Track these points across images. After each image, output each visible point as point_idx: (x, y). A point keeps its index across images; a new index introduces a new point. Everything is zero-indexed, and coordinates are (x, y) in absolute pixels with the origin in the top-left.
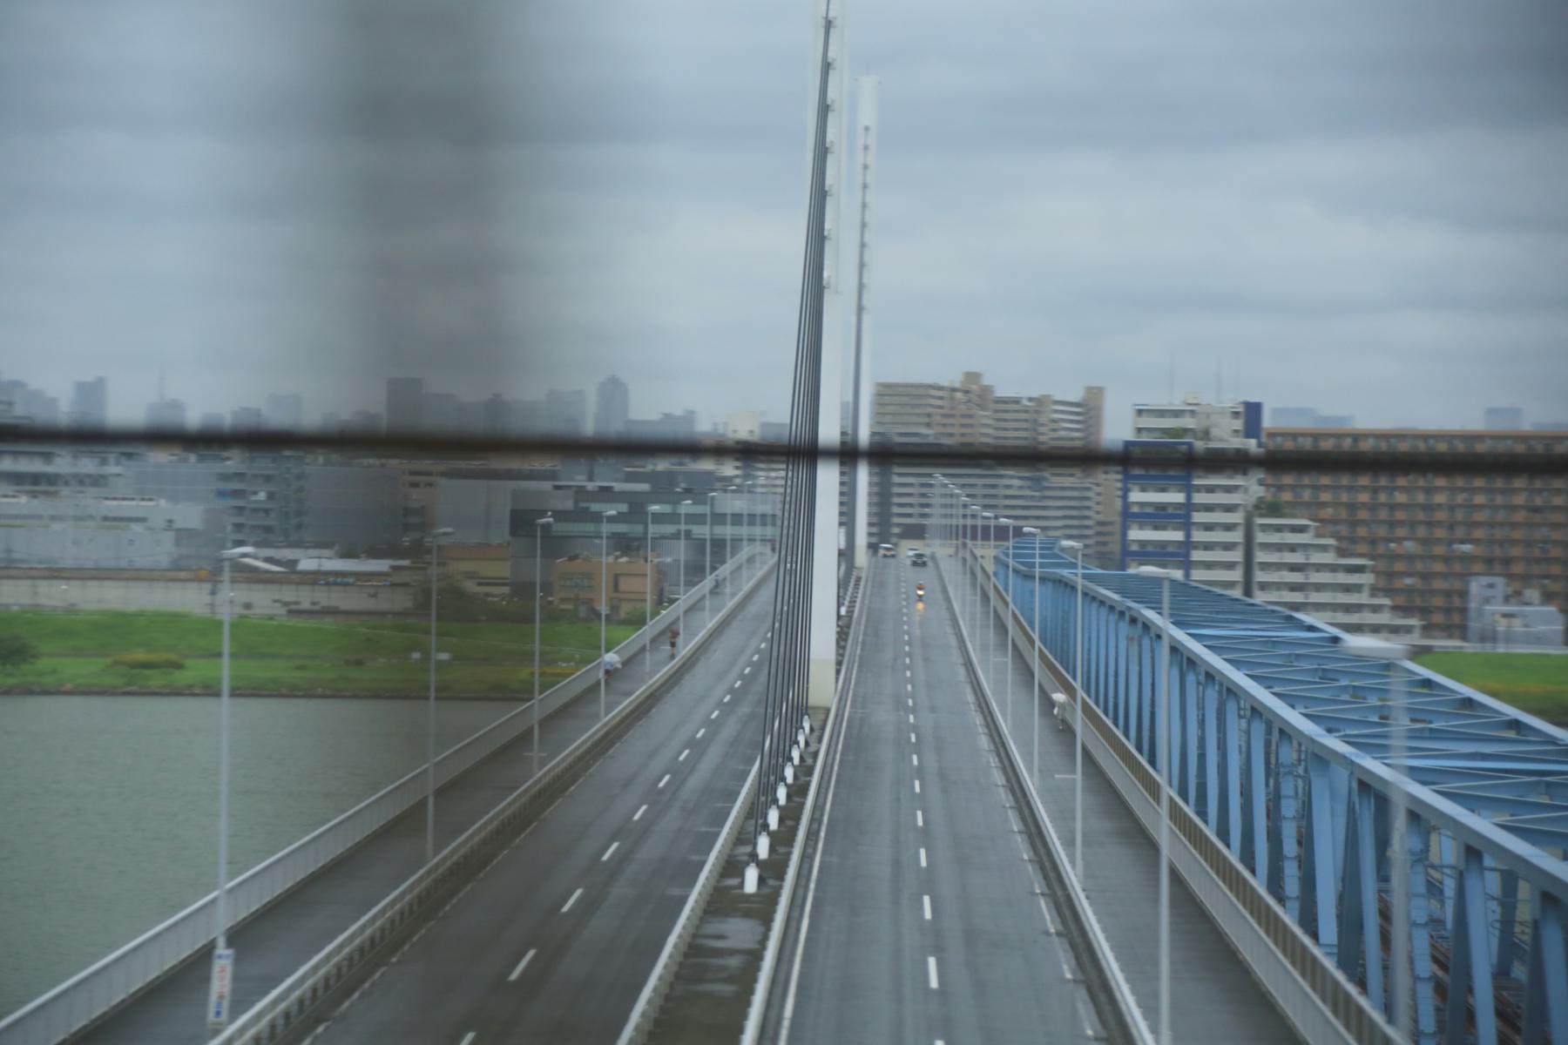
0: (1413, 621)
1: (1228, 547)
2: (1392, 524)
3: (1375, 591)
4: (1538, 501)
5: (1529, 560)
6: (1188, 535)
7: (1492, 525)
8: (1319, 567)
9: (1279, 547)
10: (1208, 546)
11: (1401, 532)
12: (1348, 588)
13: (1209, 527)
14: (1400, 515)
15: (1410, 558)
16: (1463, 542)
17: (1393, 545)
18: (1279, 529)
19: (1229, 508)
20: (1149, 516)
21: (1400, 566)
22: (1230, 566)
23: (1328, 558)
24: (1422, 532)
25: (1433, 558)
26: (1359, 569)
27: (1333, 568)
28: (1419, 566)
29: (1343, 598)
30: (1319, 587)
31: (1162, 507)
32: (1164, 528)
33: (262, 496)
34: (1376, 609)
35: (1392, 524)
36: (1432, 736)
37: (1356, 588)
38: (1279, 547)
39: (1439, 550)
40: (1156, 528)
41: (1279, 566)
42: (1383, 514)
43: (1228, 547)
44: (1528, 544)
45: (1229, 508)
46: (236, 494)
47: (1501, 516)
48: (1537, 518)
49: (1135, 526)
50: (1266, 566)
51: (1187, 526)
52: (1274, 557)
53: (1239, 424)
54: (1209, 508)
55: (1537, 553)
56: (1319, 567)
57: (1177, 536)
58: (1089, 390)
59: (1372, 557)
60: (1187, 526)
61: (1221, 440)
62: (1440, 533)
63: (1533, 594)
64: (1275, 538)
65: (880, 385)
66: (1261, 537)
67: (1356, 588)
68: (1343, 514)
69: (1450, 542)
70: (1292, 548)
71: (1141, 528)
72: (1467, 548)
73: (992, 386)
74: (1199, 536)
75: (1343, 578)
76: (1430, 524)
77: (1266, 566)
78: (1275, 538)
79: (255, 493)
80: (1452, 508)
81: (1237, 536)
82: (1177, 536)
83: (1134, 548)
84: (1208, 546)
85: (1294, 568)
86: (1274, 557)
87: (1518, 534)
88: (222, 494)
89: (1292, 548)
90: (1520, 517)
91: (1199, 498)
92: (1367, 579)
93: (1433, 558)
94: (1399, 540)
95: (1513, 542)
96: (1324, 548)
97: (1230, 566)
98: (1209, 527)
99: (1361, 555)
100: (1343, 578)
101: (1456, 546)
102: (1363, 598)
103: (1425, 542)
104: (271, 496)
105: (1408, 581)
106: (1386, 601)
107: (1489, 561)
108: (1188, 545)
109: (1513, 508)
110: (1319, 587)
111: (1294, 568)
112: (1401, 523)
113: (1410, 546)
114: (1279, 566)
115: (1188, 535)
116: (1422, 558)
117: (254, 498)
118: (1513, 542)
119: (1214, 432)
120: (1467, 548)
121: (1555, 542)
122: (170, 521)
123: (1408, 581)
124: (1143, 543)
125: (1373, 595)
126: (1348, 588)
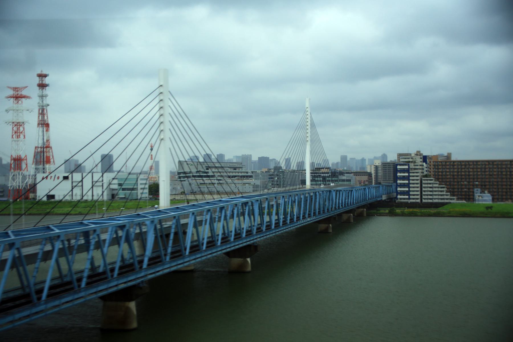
0: (455, 197)
1: (417, 184)
2: (462, 179)
3: (447, 192)
4: (491, 173)
5: (490, 185)
6: (409, 182)
7: (482, 178)
8: (435, 187)
9: (427, 184)
10: (413, 184)
11: (463, 180)
12: (441, 191)
13: (413, 180)
14: (463, 177)
15: (466, 185)
16: (476, 182)
17: (462, 183)
18: (427, 180)
19: (417, 176)
20: (402, 178)
21: (463, 187)
22: (418, 187)
23: (437, 185)
24: (468, 180)
25: (470, 185)
26: (443, 188)
27: (438, 187)
28: (467, 187)
29: (440, 193)
30: (435, 191)
31: (404, 176)
32: (405, 180)
33: (276, 178)
34: (447, 195)
35: (462, 179)
36: (317, 218)
37: (443, 191)
38: (427, 184)
39: (471, 183)
40: (403, 180)
41: (427, 187)
42: (460, 177)
43: (417, 184)
44: (490, 182)
45: (417, 176)
46: (272, 178)
47: (484, 176)
48: (491, 177)
49: (399, 180)
50: (425, 187)
51: (409, 180)
52: (426, 186)
53: (422, 160)
54: (413, 176)
55: (491, 184)
56: (435, 187)
57: (407, 182)
58: (448, 153)
59: (446, 185)
60: (409, 180)
61: (418, 163)
62: (471, 180)
63: (486, 192)
64: (426, 182)
65: (398, 154)
66: (423, 182)
67: (443, 191)
68: (452, 177)
69: (474, 182)
70: (430, 184)
71: (400, 180)
72: (477, 183)
73: (112, 154)
74: (411, 182)
75: (440, 189)
76: (469, 178)
77: (425, 187)
78: (426, 182)
79: (275, 178)
80: (474, 175)
81: (419, 182)
82: (407, 182)
83: (399, 184)
84: (413, 184)
85: (430, 187)
86: (426, 186)
87: (487, 180)
88: (269, 178)
89: (430, 184)
90: (487, 177)
91: (411, 174)
92: (445, 189)
93: (470, 185)
94: (463, 182)
95: (486, 182)
96: (436, 184)
97: (418, 187)
98: (413, 180)
99: (444, 185)
100: (440, 189)
101: (475, 183)
102: (444, 193)
103: (469, 182)
104: (278, 178)
105: (465, 190)
106: (449, 194)
107: (482, 185)
108: (409, 183)
109: (486, 175)
110: (435, 191)
111: (430, 187)
112: (463, 178)
113: (465, 183)
114: (427, 187)
115: (409, 182)
116: (468, 185)
117: (275, 179)
118: (486, 182)
119: (416, 161)
120: (477, 183)
121: (495, 182)
122: (255, 184)
123: (465, 190)
124: (400, 183)
125: (446, 193)
126: (441, 191)
